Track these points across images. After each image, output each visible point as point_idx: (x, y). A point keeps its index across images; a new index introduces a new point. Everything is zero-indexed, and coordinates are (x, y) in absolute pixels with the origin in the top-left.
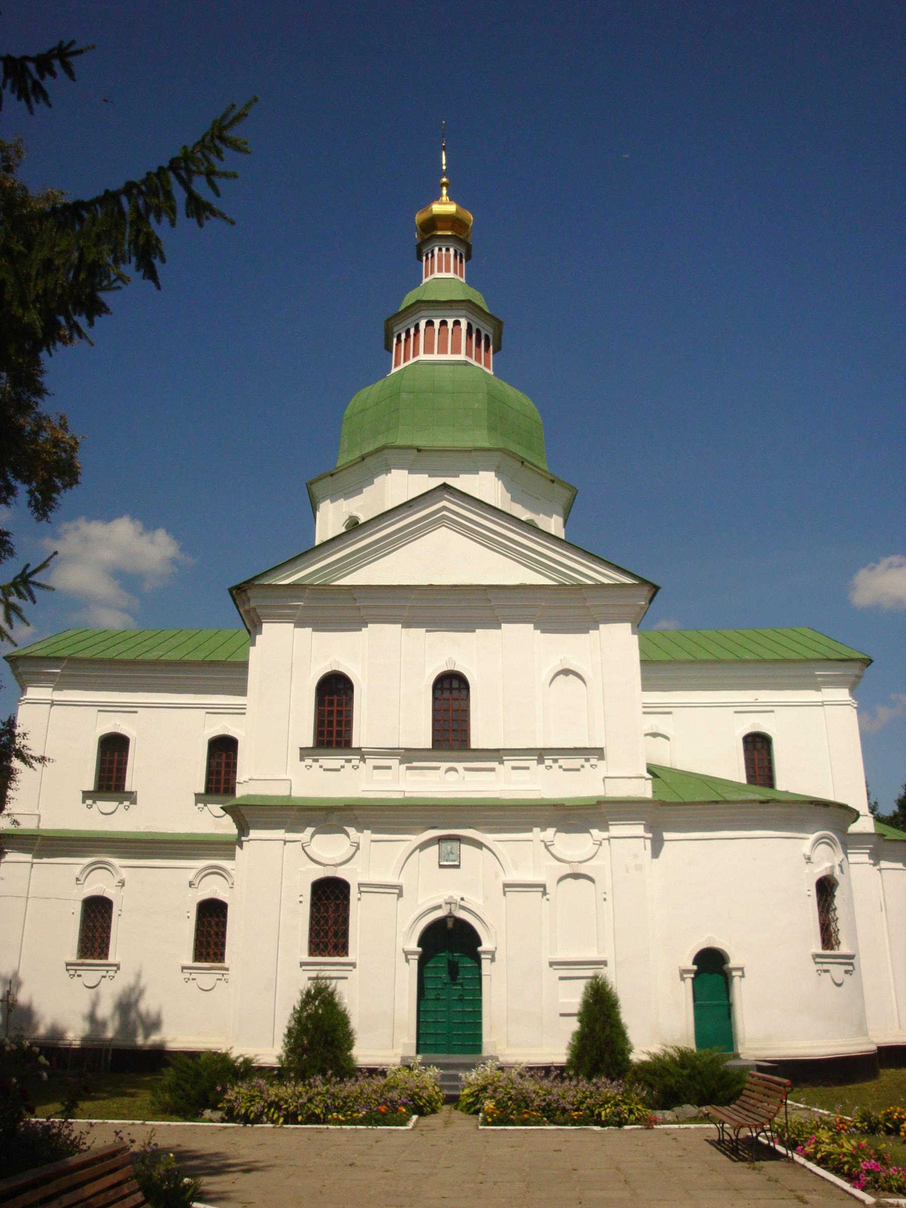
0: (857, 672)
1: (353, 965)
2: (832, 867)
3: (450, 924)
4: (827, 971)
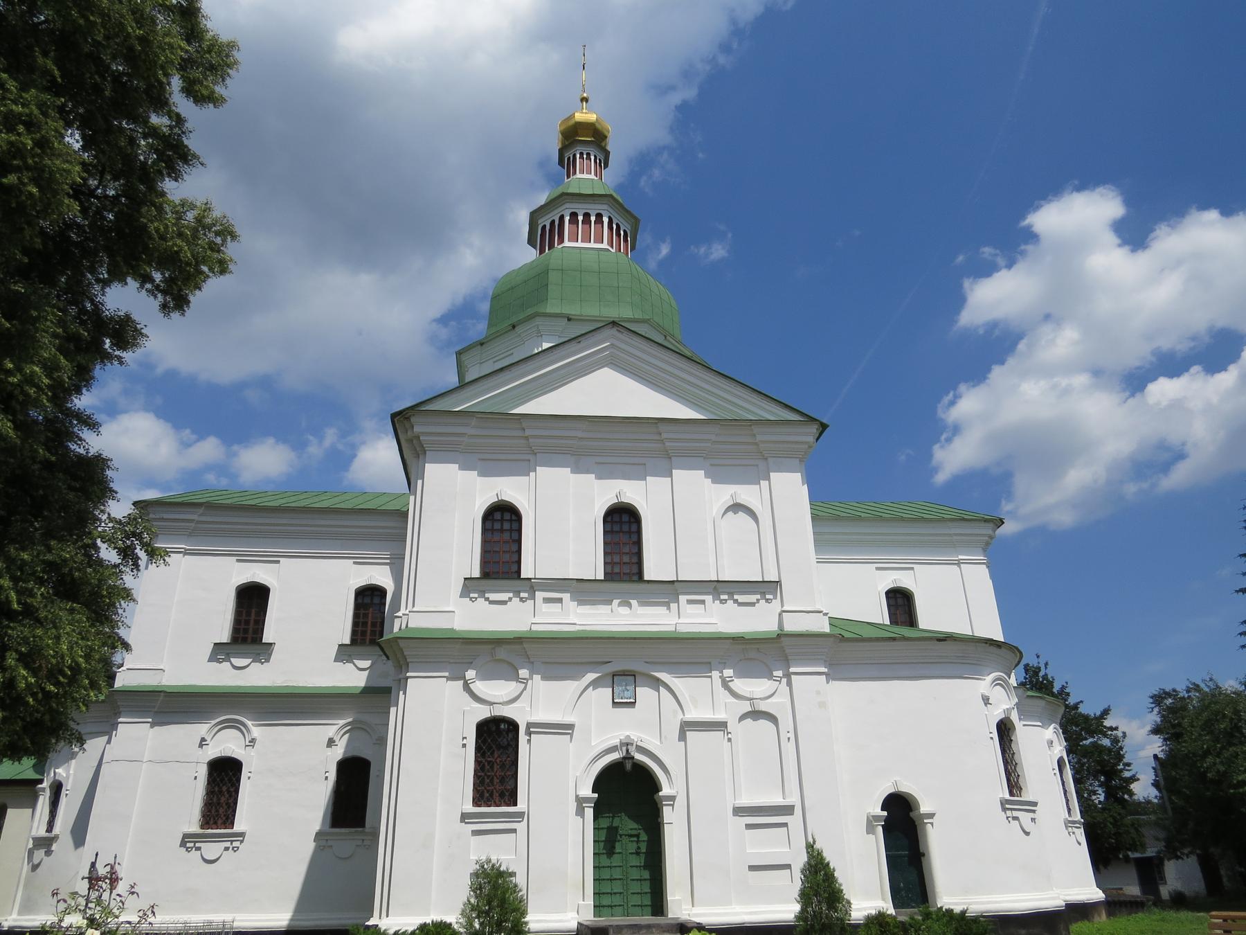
0: (990, 532)
1: (521, 815)
2: (1009, 710)
3: (628, 766)
4: (1016, 818)
